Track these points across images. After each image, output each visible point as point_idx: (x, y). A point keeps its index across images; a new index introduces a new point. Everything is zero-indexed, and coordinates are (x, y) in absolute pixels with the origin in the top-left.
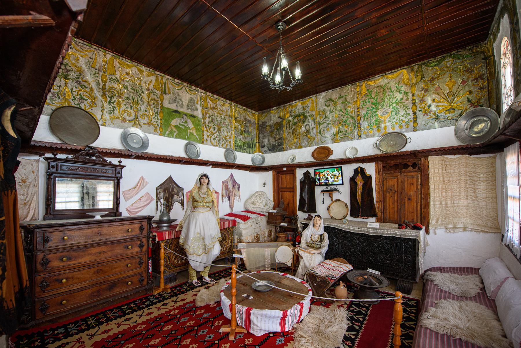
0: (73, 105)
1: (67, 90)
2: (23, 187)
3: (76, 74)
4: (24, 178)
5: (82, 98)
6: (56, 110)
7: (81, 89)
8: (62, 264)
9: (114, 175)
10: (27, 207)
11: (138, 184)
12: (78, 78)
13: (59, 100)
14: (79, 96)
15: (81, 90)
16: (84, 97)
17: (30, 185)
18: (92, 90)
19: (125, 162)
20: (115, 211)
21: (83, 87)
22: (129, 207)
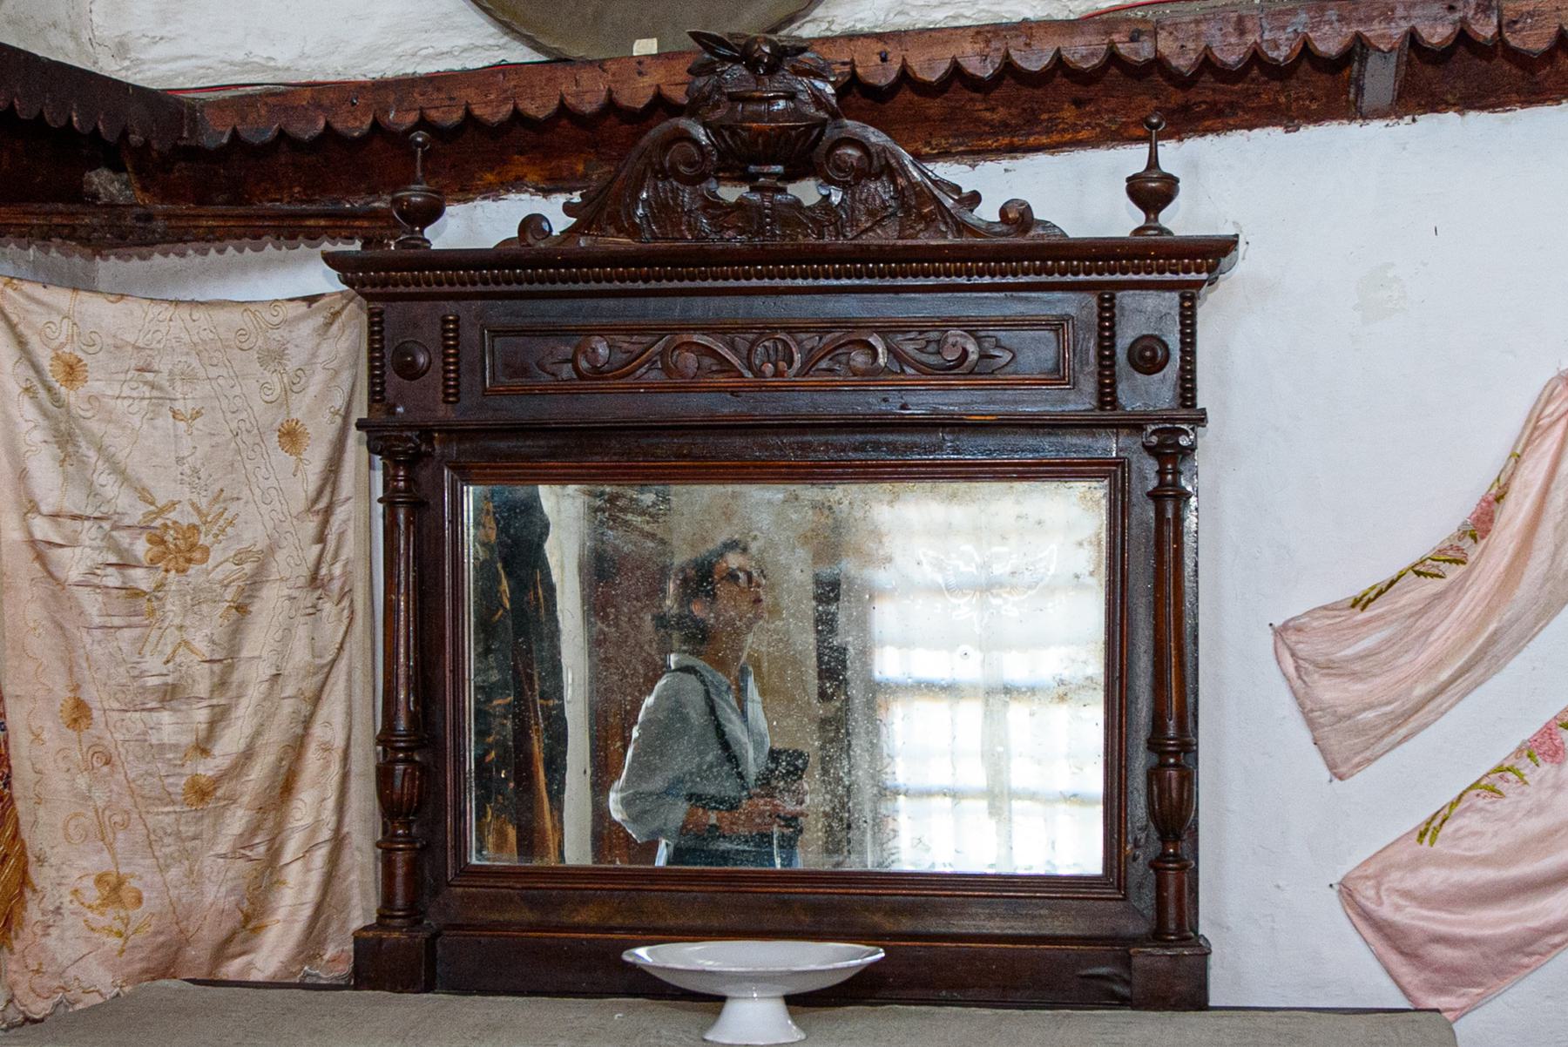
2: (172, 606)
4: (184, 516)
9: (1081, 401)
10: (237, 821)
11: (1480, 526)
17: (255, 583)
19: (1226, 178)
22: (1379, 867)
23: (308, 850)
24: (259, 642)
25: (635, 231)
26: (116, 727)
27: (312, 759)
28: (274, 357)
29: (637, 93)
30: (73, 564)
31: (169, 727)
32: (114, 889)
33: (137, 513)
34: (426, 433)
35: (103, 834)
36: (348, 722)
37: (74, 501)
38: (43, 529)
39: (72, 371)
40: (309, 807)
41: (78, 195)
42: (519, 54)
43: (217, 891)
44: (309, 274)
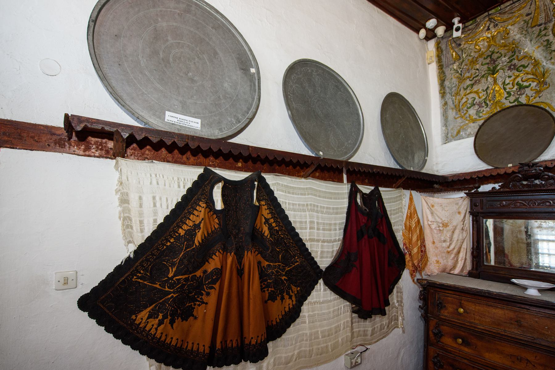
0: (508, 104)
1: (497, 89)
2: (445, 232)
3: (507, 58)
5: (521, 88)
6: (483, 124)
7: (517, 73)
8: (455, 345)
10: (453, 256)
12: (511, 61)
13: (488, 109)
14: (516, 87)
15: (518, 76)
16: (525, 84)
17: (455, 229)
18: (537, 63)
20: (212, 258)
21: (521, 68)
23: (462, 260)
24: (455, 236)
25: (509, 188)
26: (438, 244)
27: (462, 249)
28: (457, 204)
29: (510, 171)
30: (433, 227)
31: (444, 245)
32: (438, 262)
33: (440, 221)
34: (478, 213)
35: (436, 256)
36: (467, 245)
37: (433, 220)
38: (430, 223)
39: (433, 206)
40: (462, 255)
41: (433, 188)
42: (490, 167)
43: (450, 263)
44: (462, 194)
